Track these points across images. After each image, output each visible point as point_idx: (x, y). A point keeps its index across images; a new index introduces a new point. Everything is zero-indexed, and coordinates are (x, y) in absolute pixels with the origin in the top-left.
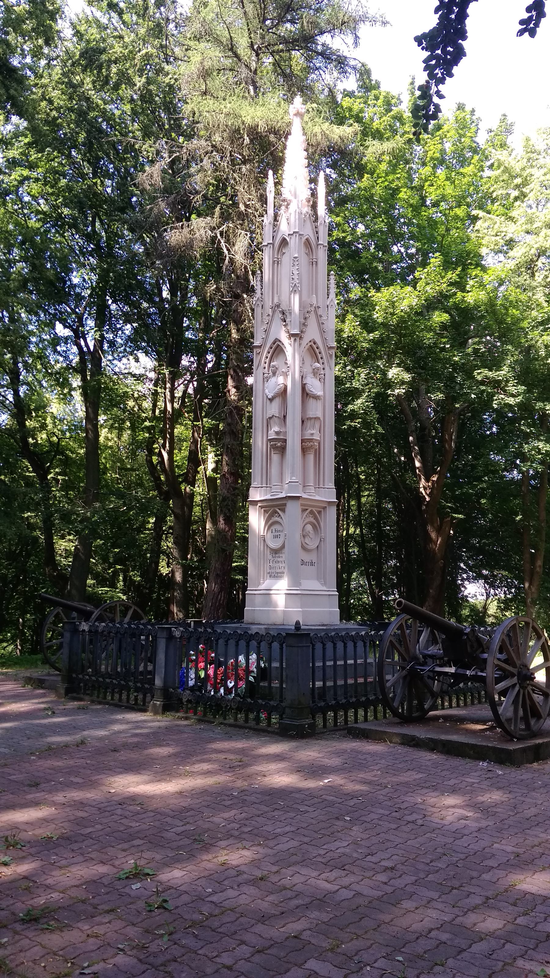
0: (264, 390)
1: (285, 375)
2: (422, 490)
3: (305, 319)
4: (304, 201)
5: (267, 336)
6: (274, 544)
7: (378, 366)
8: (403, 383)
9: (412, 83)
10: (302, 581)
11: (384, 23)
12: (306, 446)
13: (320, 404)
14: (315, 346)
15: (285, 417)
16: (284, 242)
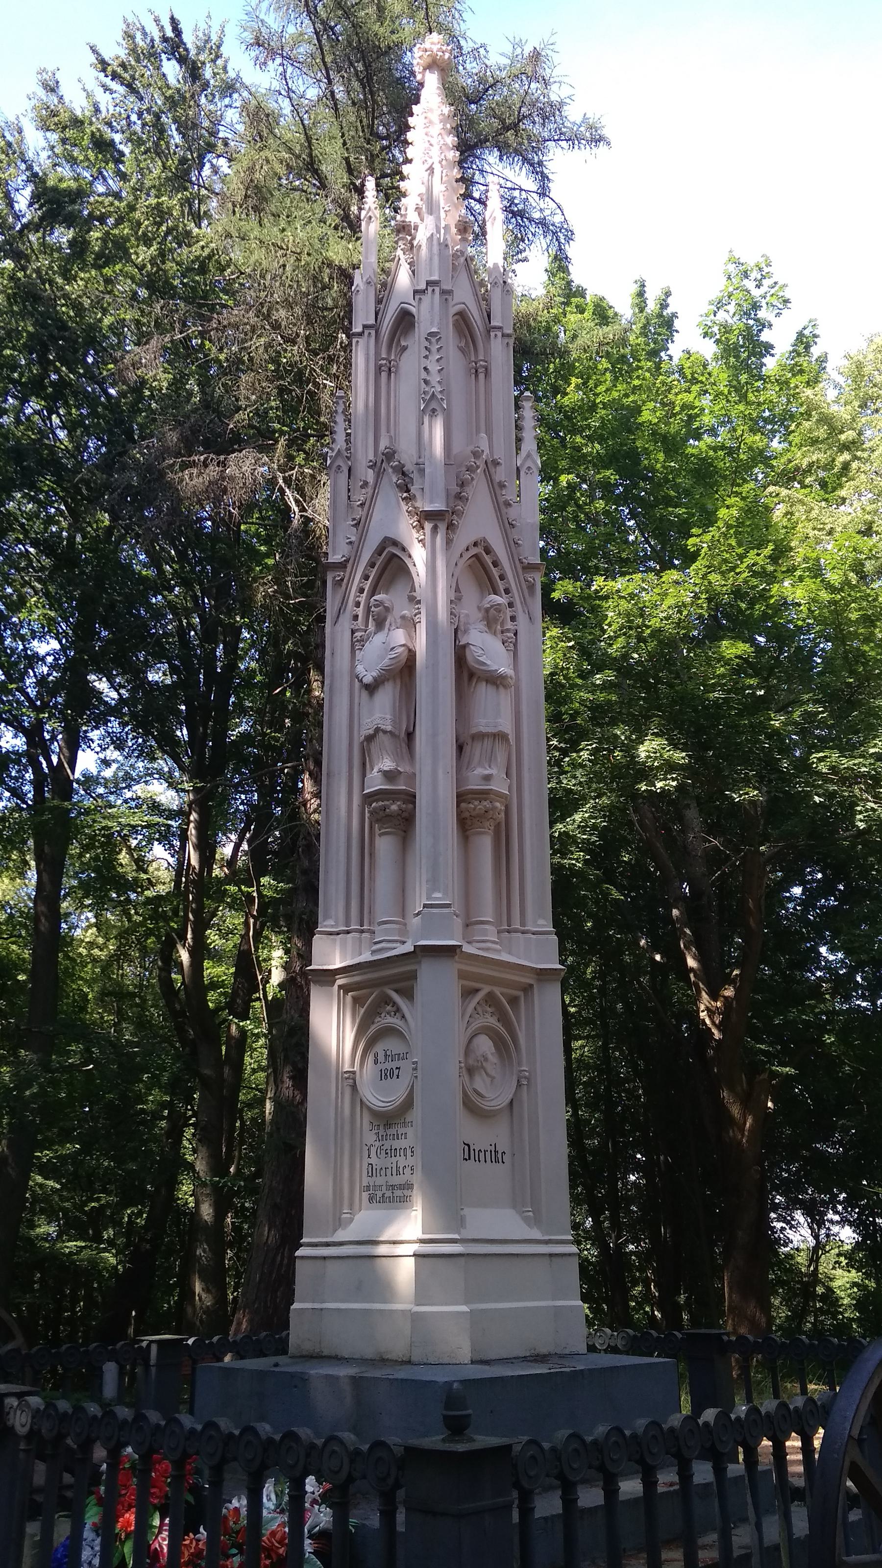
0: (353, 667)
1: (410, 624)
2: (703, 1015)
3: (462, 484)
4: (454, 230)
5: (362, 538)
6: (378, 1097)
7: (616, 737)
8: (670, 767)
9: (641, 294)
10: (467, 1211)
11: (598, 140)
12: (472, 813)
13: (505, 699)
14: (488, 559)
15: (410, 736)
16: (405, 321)
